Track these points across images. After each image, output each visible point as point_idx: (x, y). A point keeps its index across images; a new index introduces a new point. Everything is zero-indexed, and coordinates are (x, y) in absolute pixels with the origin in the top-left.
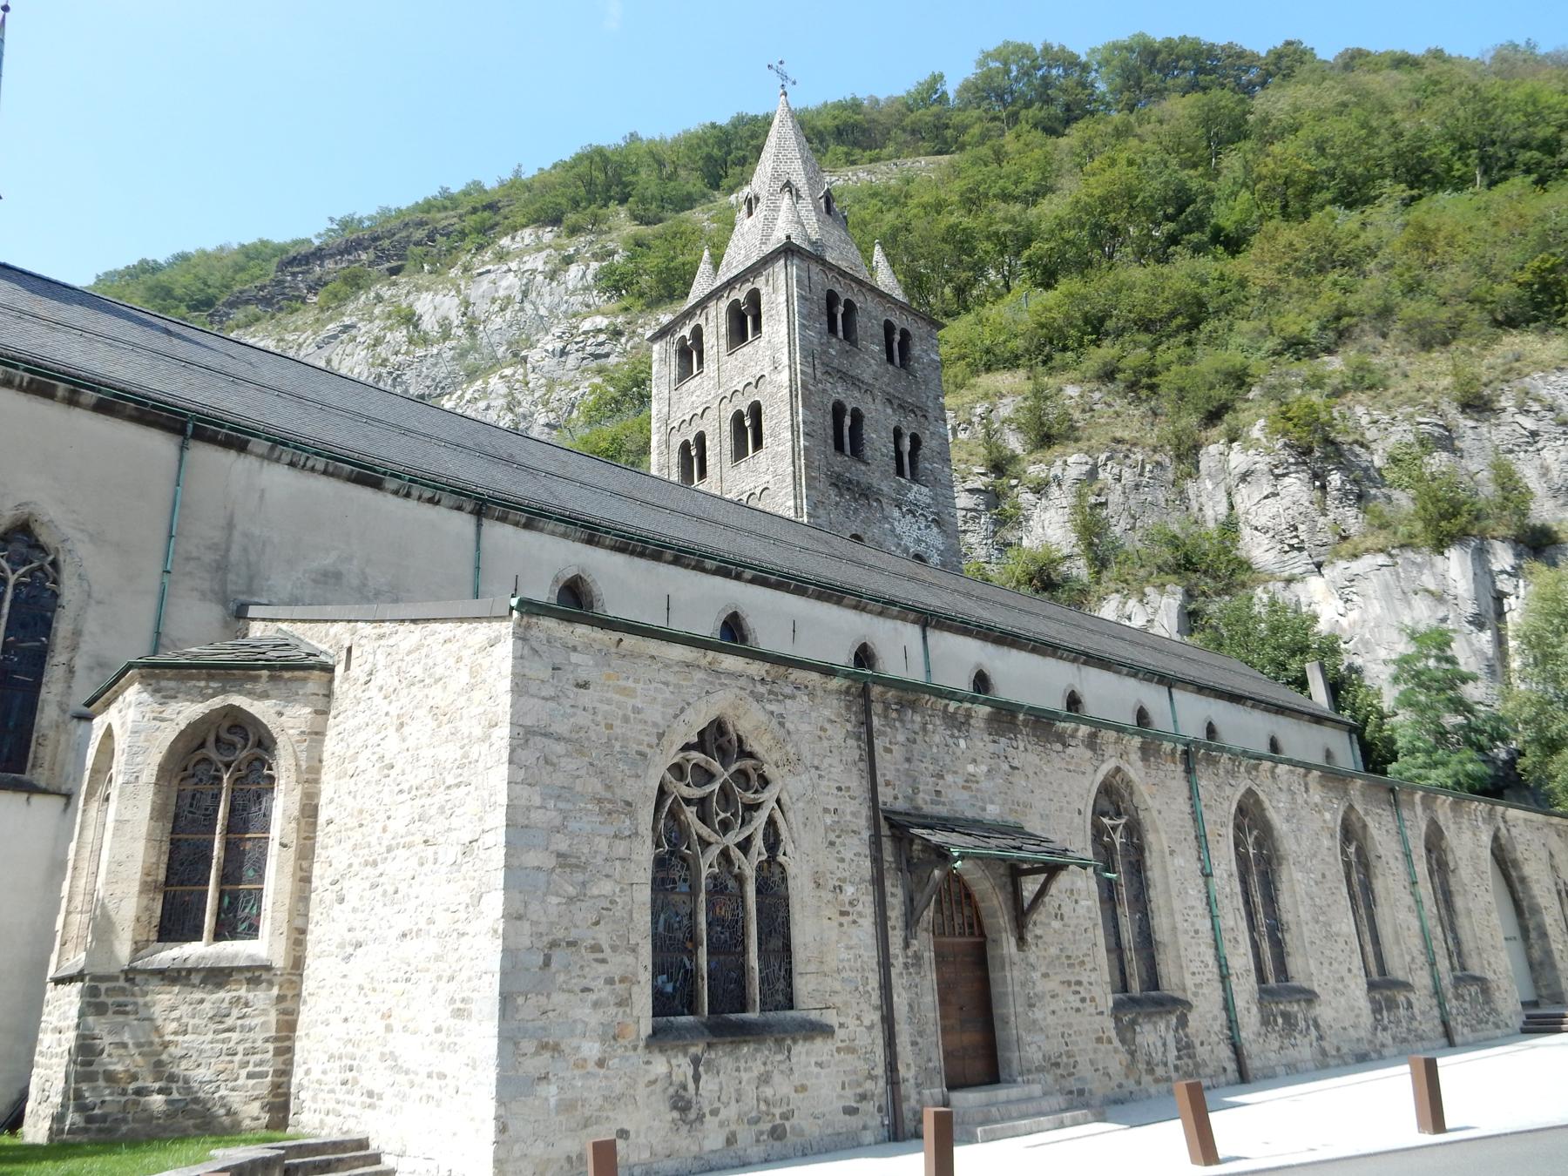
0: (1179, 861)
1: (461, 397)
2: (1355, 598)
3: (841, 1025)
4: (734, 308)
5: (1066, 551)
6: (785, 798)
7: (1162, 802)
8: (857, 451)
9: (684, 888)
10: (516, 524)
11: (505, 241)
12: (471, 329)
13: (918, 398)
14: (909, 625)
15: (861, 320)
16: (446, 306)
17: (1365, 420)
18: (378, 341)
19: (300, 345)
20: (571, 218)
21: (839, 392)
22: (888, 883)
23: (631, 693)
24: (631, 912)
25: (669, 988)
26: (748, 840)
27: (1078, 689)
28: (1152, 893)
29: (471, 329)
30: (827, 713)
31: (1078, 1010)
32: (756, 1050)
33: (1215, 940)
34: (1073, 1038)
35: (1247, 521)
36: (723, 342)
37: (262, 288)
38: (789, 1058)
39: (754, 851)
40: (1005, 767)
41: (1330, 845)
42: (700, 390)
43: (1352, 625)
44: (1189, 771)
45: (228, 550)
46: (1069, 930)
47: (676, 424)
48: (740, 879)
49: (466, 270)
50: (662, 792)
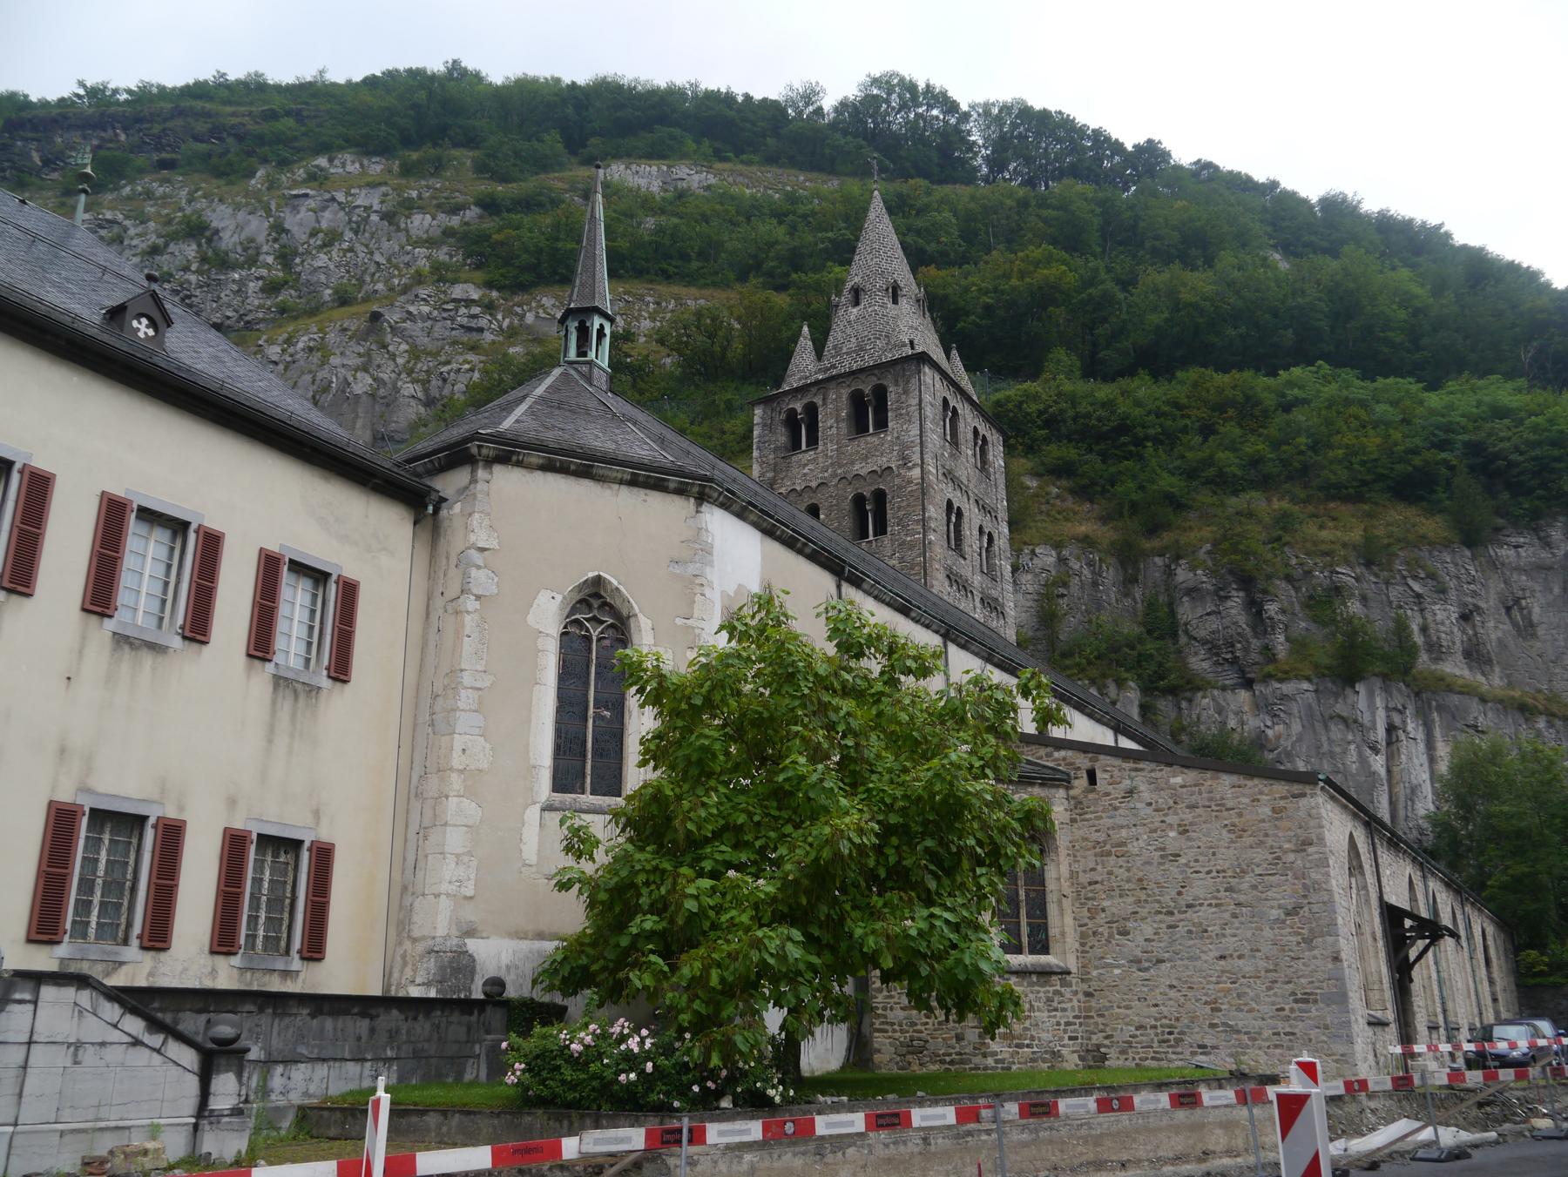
11: (322, 161)
17: (1294, 561)
29: (285, 258)
35: (1186, 632)
43: (1278, 737)
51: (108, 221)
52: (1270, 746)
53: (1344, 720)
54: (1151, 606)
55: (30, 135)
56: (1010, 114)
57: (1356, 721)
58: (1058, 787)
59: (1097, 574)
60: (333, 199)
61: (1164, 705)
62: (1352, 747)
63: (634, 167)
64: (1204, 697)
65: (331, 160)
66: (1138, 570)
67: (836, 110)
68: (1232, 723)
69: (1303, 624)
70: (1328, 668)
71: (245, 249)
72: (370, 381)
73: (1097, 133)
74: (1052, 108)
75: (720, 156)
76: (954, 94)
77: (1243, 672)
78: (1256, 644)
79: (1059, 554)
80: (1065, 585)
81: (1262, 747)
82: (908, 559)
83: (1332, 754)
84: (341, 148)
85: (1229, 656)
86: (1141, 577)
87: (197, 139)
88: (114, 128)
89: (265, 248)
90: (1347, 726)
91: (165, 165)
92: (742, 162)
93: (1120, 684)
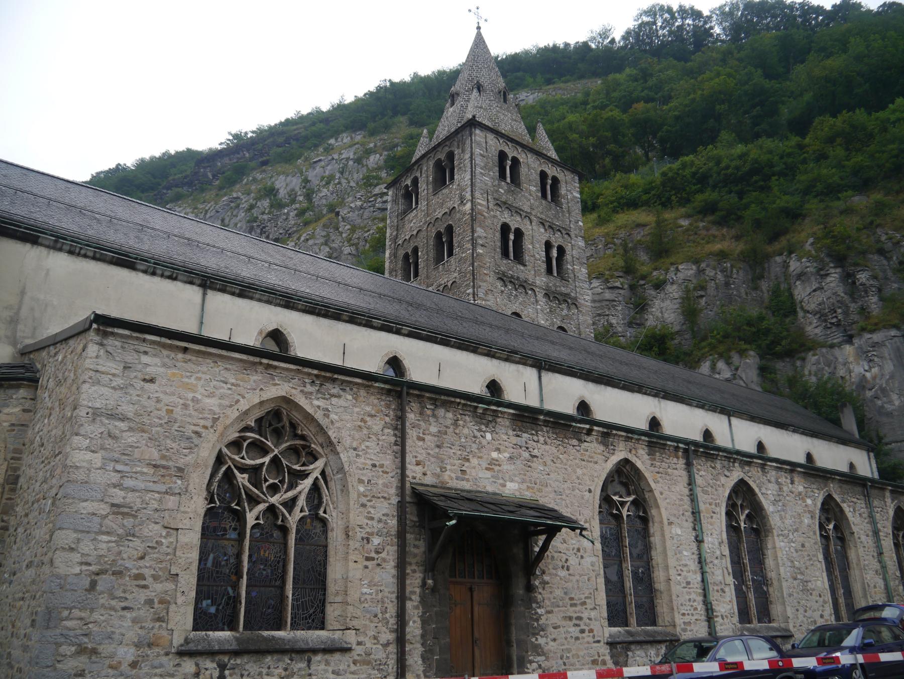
1: (299, 239)
2: (876, 359)
3: (359, 643)
4: (438, 164)
5: (676, 328)
6: (328, 471)
7: (666, 483)
8: (519, 257)
9: (234, 535)
10: (233, 294)
11: (332, 141)
12: (309, 196)
14: (529, 369)
15: (523, 170)
16: (294, 183)
17: (883, 238)
18: (252, 207)
19: (206, 211)
20: (371, 125)
21: (505, 217)
22: (408, 536)
23: (193, 389)
24: (175, 549)
25: (213, 610)
26: (294, 500)
27: (658, 416)
28: (653, 553)
29: (309, 196)
30: (368, 409)
31: (577, 638)
32: (279, 660)
33: (704, 590)
34: (572, 660)
35: (802, 308)
36: (430, 186)
37: (186, 177)
38: (309, 666)
39: (297, 509)
41: (810, 523)
42: (415, 221)
43: (874, 378)
44: (689, 465)
45: (19, 308)
46: (574, 579)
47: (400, 242)
48: (284, 530)
49: (306, 159)
50: (220, 459)
52: (869, 386)
54: (776, 292)
55: (207, 165)
58: (18, 387)
60: (333, 159)
61: (783, 368)
64: (814, 355)
65: (336, 139)
66: (763, 269)
67: (624, 38)
68: (841, 372)
69: (895, 286)
72: (328, 249)
75: (549, 82)
76: (697, 7)
78: (853, 306)
79: (698, 267)
80: (703, 288)
81: (864, 388)
82: (463, 270)
84: (343, 132)
85: (834, 320)
86: (766, 274)
87: (278, 146)
89: (299, 193)
91: (265, 163)
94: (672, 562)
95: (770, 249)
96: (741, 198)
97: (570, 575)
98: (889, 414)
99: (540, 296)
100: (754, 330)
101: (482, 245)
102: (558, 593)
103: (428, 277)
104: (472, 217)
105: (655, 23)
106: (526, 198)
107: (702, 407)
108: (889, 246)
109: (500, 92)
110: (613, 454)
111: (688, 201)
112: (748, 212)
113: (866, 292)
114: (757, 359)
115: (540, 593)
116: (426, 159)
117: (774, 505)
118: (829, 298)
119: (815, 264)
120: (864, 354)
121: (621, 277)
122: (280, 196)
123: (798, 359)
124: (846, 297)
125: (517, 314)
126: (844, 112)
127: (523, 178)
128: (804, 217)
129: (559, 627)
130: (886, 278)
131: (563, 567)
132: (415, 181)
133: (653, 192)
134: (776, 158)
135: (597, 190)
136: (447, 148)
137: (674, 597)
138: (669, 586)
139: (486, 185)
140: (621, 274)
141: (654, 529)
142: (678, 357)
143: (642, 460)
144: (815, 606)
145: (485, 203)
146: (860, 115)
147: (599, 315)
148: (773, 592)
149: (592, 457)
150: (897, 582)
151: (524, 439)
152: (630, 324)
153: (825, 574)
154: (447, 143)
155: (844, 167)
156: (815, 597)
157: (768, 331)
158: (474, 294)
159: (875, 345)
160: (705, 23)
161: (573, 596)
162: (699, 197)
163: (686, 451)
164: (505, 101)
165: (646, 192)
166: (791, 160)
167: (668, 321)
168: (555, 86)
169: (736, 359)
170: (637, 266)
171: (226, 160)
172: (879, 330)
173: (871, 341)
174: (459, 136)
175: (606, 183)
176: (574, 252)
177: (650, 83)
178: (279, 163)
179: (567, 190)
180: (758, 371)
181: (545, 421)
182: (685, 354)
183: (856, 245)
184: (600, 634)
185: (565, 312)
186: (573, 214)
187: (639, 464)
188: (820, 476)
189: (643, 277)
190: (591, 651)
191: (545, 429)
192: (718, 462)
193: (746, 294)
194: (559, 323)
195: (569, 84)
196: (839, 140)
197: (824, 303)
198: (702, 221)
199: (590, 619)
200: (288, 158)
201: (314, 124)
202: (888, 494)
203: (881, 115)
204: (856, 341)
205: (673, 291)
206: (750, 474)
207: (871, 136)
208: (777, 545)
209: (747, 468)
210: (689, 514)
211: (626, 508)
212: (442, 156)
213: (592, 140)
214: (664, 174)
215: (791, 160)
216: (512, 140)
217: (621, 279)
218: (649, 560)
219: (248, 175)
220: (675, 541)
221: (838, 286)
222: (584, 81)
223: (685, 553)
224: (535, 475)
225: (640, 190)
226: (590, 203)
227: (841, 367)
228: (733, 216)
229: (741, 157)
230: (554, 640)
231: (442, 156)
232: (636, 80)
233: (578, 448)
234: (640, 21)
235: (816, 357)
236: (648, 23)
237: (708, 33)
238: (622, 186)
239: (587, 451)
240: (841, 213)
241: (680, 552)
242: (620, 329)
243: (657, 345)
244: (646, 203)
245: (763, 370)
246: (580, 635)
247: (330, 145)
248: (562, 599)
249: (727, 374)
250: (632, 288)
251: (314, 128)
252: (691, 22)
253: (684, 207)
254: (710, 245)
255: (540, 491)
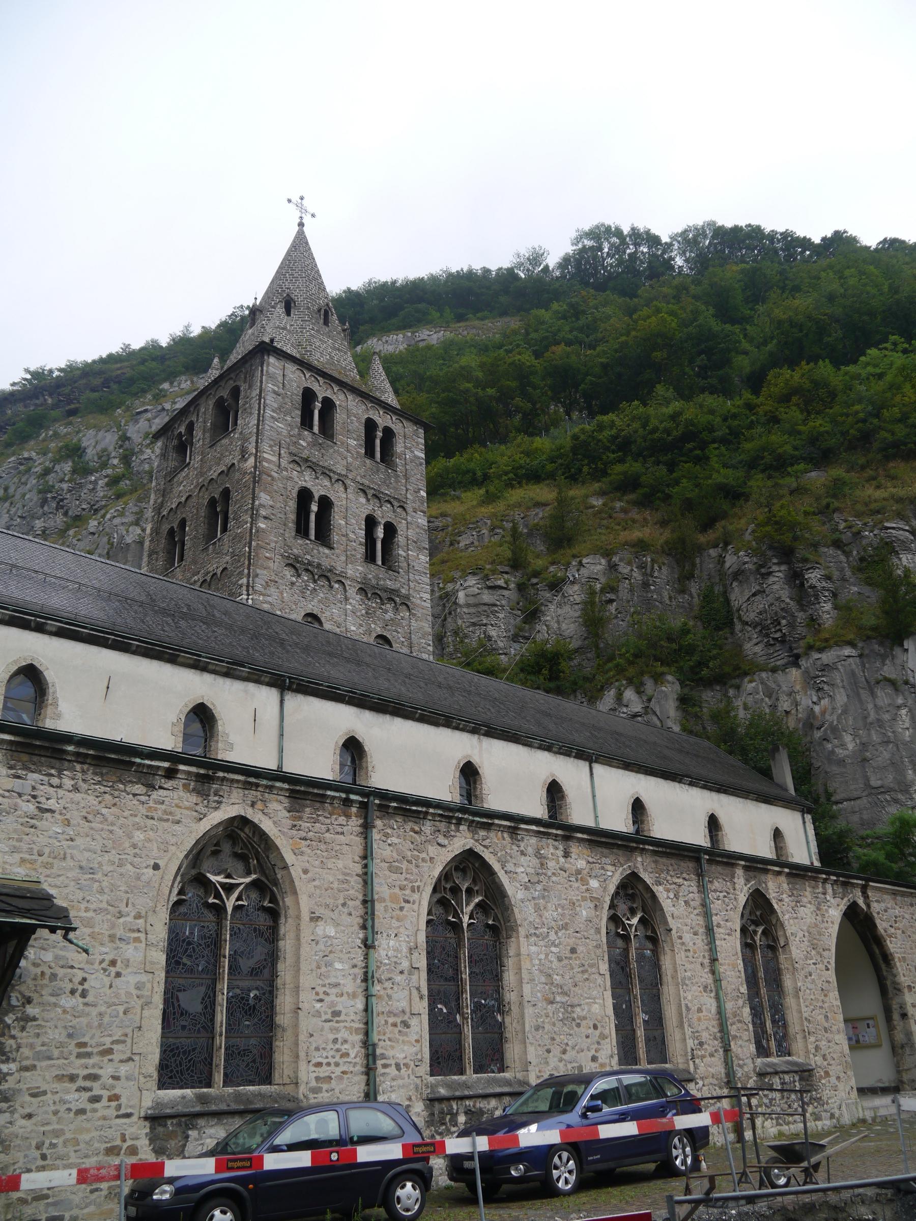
0: (327, 929)
1: (103, 516)
2: (826, 687)
8: (323, 536)
11: (166, 386)
13: (396, 489)
15: (339, 417)
16: (107, 440)
21: (307, 480)
27: (476, 760)
28: (280, 966)
29: (126, 459)
31: (82, 1111)
33: (367, 1023)
34: (61, 1150)
35: (740, 618)
36: (208, 435)
40: (31, 808)
43: (823, 713)
44: (367, 827)
46: (94, 1012)
47: (165, 513)
51: (25, 459)
52: (817, 724)
53: (892, 683)
54: (707, 597)
56: (705, 236)
57: (906, 683)
59: (648, 574)
60: (163, 409)
61: (710, 698)
62: (904, 712)
63: (384, 339)
64: (751, 682)
66: (694, 565)
70: (873, 629)
71: (100, 458)
73: (786, 235)
74: (742, 223)
75: (460, 318)
76: (655, 231)
77: (791, 649)
78: (801, 616)
79: (609, 561)
80: (613, 590)
81: (811, 726)
83: (880, 723)
84: (181, 373)
85: (778, 635)
87: (93, 390)
88: (43, 396)
89: (113, 454)
90: (897, 690)
91: (73, 413)
92: (478, 319)
93: (658, 678)
94: (306, 980)
95: (702, 539)
96: (671, 471)
97: (86, 1004)
98: (841, 762)
99: (352, 591)
100: (674, 646)
101: (265, 518)
102: (55, 1035)
103: (194, 562)
104: (254, 477)
105: (600, 249)
106: (340, 454)
107: (549, 749)
108: (847, 537)
109: (319, 311)
110: (216, 809)
111: (605, 473)
112: (676, 489)
113: (817, 597)
114: (677, 687)
115: (13, 1037)
116: (205, 397)
117: (527, 888)
118: (772, 604)
119: (755, 560)
120: (813, 682)
121: (507, 573)
122: (87, 458)
123: (731, 687)
124: (792, 602)
125: (313, 617)
126: (804, 363)
127: (338, 427)
128: (747, 497)
129: (45, 1093)
130: (844, 580)
131: (73, 992)
132: (190, 427)
133: (560, 461)
134: (718, 419)
135: (490, 456)
136: (231, 382)
137: (302, 1037)
138: (297, 1019)
139: (279, 433)
140: (507, 569)
141: (286, 928)
142: (575, 683)
143: (273, 818)
144: (585, 1043)
145: (275, 459)
146: (825, 369)
147: (474, 624)
148: (511, 1024)
149: (171, 813)
150: (740, 1002)
151: (30, 783)
152: (515, 638)
153: (608, 994)
154: (232, 375)
155: (799, 433)
156: (583, 1030)
157: (691, 650)
158: (248, 586)
159: (825, 668)
160: (664, 252)
161: (85, 1039)
162: (619, 468)
163: (364, 806)
164: (326, 323)
165: (552, 460)
166: (736, 422)
167: (566, 634)
168: (468, 323)
169: (649, 685)
170: (530, 558)
171: (20, 407)
172: (830, 647)
173: (819, 663)
174: (247, 365)
175: (503, 447)
176: (410, 533)
177: (582, 321)
178: (91, 413)
179: (406, 447)
180: (677, 703)
181: (78, 754)
182: (586, 679)
183: (807, 535)
184: (135, 1101)
185: (390, 615)
186: (413, 479)
187: (267, 826)
188: (619, 847)
189: (536, 574)
190: (109, 1133)
191: (78, 767)
192: (428, 823)
193: (670, 598)
194: (379, 631)
195: (487, 321)
196: (794, 399)
197: (766, 612)
198: (620, 500)
199: (116, 1078)
200: (104, 408)
201: (143, 362)
202: (739, 872)
203: (851, 368)
204: (803, 662)
205: (575, 592)
206: (486, 843)
207: (833, 395)
208: (523, 950)
209: (482, 833)
210: (358, 903)
211: (235, 895)
212: (225, 393)
213: (490, 391)
214: (575, 437)
215: (736, 422)
216: (324, 375)
217: (506, 576)
218: (274, 975)
219: (48, 428)
220: (321, 946)
221: (782, 589)
222: (507, 319)
223: (338, 966)
224: (42, 840)
225: (544, 457)
226: (479, 474)
227: (786, 698)
228: (659, 495)
229: (674, 417)
230: (29, 1116)
231: (225, 393)
232: (564, 317)
233: (143, 798)
234: (580, 246)
235: (754, 684)
236: (592, 248)
237: (668, 264)
238: (522, 453)
239: (163, 803)
240: (792, 493)
241: (329, 964)
242: (501, 644)
243: (546, 670)
244: (551, 476)
245: (684, 701)
246: (89, 1106)
247: (161, 391)
248: (61, 1045)
249: (637, 707)
250: (521, 588)
251: (142, 368)
252: (645, 250)
253: (599, 481)
254: (626, 533)
255: (47, 865)
